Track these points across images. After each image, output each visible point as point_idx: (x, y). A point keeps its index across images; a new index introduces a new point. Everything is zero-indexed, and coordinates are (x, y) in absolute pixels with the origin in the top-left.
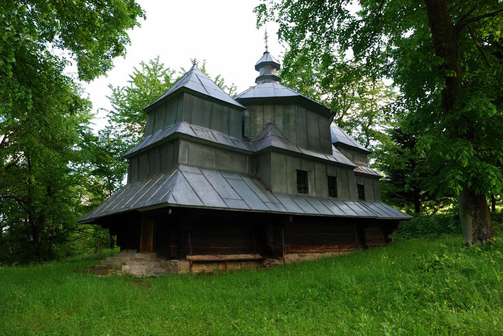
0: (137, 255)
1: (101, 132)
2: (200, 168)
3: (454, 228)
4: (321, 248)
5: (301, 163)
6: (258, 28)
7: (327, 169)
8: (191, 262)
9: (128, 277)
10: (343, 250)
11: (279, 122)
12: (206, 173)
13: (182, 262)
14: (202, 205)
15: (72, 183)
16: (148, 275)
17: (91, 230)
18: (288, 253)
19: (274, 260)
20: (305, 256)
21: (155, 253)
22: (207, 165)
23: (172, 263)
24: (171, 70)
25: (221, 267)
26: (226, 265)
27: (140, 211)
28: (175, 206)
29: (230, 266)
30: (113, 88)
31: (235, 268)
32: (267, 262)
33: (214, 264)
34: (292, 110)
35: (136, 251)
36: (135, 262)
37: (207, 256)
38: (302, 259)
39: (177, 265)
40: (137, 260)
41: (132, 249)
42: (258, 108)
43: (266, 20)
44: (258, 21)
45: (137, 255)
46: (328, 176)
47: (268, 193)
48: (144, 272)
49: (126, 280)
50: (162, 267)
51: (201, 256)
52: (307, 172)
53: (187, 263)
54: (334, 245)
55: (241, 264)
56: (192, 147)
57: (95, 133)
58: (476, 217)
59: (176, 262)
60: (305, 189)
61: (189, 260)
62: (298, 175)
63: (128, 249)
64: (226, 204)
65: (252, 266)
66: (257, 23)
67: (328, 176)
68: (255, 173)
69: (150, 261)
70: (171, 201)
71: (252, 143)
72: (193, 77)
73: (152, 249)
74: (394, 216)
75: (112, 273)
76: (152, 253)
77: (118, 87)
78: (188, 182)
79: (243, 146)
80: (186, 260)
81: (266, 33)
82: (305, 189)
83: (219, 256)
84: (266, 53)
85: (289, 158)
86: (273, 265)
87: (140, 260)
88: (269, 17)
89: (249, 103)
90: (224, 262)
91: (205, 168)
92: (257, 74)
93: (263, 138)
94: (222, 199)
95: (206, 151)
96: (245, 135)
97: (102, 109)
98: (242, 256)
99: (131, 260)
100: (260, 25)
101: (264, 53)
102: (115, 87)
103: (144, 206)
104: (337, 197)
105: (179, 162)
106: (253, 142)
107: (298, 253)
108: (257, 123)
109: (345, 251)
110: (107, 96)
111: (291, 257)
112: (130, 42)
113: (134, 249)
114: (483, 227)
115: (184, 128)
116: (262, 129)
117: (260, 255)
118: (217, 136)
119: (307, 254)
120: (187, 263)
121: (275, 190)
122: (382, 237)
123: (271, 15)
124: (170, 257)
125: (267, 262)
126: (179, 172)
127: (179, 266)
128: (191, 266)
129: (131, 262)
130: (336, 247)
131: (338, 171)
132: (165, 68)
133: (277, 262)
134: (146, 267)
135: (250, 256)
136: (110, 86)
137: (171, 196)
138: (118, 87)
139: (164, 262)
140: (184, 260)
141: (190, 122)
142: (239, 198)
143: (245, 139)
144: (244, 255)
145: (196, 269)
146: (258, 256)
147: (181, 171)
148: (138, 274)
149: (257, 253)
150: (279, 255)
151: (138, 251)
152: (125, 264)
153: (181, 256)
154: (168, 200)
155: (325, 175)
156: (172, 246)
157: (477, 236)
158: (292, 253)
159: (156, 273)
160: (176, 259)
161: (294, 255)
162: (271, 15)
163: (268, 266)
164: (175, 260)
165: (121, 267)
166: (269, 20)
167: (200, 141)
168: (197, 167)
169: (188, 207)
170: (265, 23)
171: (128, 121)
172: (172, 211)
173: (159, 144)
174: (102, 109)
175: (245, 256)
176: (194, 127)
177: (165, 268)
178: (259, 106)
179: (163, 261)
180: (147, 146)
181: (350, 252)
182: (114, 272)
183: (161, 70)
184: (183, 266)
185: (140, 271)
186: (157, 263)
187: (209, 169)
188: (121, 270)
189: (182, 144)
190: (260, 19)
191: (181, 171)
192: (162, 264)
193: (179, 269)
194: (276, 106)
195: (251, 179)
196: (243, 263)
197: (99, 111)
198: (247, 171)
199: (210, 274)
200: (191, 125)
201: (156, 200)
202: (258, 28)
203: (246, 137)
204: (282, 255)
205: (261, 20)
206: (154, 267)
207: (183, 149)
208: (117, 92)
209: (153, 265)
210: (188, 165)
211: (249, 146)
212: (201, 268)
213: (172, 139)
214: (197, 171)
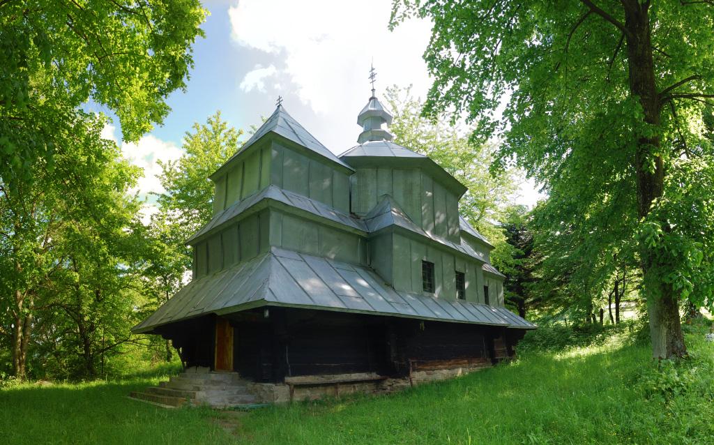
0: (213, 376)
1: (155, 218)
2: (299, 252)
3: (575, 339)
4: (450, 363)
5: (427, 251)
6: (392, 29)
7: (455, 263)
8: (292, 386)
9: (206, 411)
10: (473, 364)
11: (399, 195)
12: (308, 259)
13: (278, 387)
14: (312, 304)
15: (123, 287)
16: (230, 405)
17: (145, 340)
18: (414, 370)
19: (398, 380)
20: (435, 373)
21: (236, 373)
22: (307, 249)
23: (264, 388)
24: (237, 130)
25: (329, 391)
26: (337, 388)
27: (219, 314)
28: (275, 305)
29: (341, 390)
30: (163, 164)
31: (348, 392)
32: (389, 384)
33: (320, 388)
34: (417, 178)
35: (208, 369)
36: (212, 387)
37: (311, 376)
38: (430, 378)
39: (272, 392)
40: (214, 383)
41: (204, 366)
42: (370, 172)
43: (405, 15)
44: (393, 15)
45: (213, 375)
46: (456, 272)
47: (389, 288)
48: (227, 402)
49: (203, 416)
50: (250, 392)
51: (304, 377)
52: (433, 264)
53: (287, 388)
54: (463, 359)
55: (354, 387)
56: (287, 220)
57: (146, 222)
58: (670, 329)
59: (269, 387)
60: (431, 287)
61: (289, 384)
62: (424, 267)
63: (197, 366)
64: (344, 303)
65: (368, 388)
66: (391, 20)
67: (456, 272)
68: (368, 263)
69: (232, 384)
70: (269, 297)
71: (363, 222)
72: (280, 122)
73: (232, 367)
74: (514, 325)
75: (182, 404)
76: (233, 373)
77: (170, 161)
78: (287, 271)
79: (351, 224)
80: (284, 383)
81: (373, 69)
82: (431, 287)
83: (326, 376)
84: (373, 98)
85: (414, 244)
86: (397, 387)
87: (219, 382)
88: (411, 10)
89: (355, 165)
90: (326, 385)
91: (305, 254)
92: (361, 130)
93: (379, 215)
94: (336, 295)
95: (305, 228)
96: (352, 211)
97: (151, 193)
98: (355, 376)
99: (206, 383)
100: (396, 23)
101: (370, 99)
102: (165, 162)
103: (226, 306)
104: (465, 299)
105: (271, 243)
106: (364, 220)
107: (425, 370)
108: (369, 194)
109: (475, 366)
110: (156, 176)
111: (418, 376)
112: (192, 62)
113: (206, 366)
114: (677, 340)
115: (275, 194)
116: (376, 203)
117: (378, 374)
118: (318, 208)
119: (436, 371)
120: (287, 388)
121: (397, 285)
122: (505, 348)
123: (414, 7)
124: (260, 378)
125: (387, 383)
126: (273, 258)
127: (275, 393)
128: (292, 393)
129: (207, 387)
130: (466, 361)
131: (467, 266)
132: (228, 127)
133: (402, 383)
134: (227, 392)
135: (364, 376)
136: (159, 162)
137: (268, 291)
138: (170, 161)
139: (252, 386)
140: (281, 384)
141: (282, 187)
142: (357, 295)
143: (353, 215)
144: (357, 374)
145: (299, 396)
146: (375, 376)
147: (275, 256)
148: (219, 404)
149: (374, 371)
150: (404, 373)
151: (212, 369)
152: (199, 389)
153: (277, 378)
154: (264, 295)
155: (453, 269)
156: (265, 365)
157: (671, 349)
158: (419, 370)
159: (242, 402)
160: (270, 382)
161: (421, 372)
162: (414, 7)
163: (389, 388)
164: (269, 384)
165: (194, 393)
166: (411, 15)
167: (299, 213)
168: (294, 251)
169: (294, 307)
170: (403, 20)
171: (186, 205)
172: (270, 313)
173: (238, 220)
174: (151, 193)
175: (360, 376)
176: (287, 193)
177: (254, 394)
178: (370, 170)
179: (250, 385)
180: (220, 225)
181: (480, 368)
182: (186, 402)
183: (223, 132)
184: (280, 392)
185: (220, 398)
186: (242, 387)
187: (310, 254)
188: (194, 398)
189: (274, 217)
190: (396, 11)
191: (275, 256)
192: (249, 389)
193: (275, 397)
194: (395, 172)
195: (364, 270)
196: (356, 385)
197: (149, 198)
198: (358, 259)
199: (320, 403)
200: (283, 190)
201: (243, 298)
202: (392, 29)
203: (354, 214)
204: (408, 374)
205: (398, 14)
206: (238, 393)
207: (276, 228)
208: (168, 170)
209: (237, 390)
210: (281, 247)
211: (359, 224)
212: (303, 394)
213: (258, 210)
214: (296, 256)
